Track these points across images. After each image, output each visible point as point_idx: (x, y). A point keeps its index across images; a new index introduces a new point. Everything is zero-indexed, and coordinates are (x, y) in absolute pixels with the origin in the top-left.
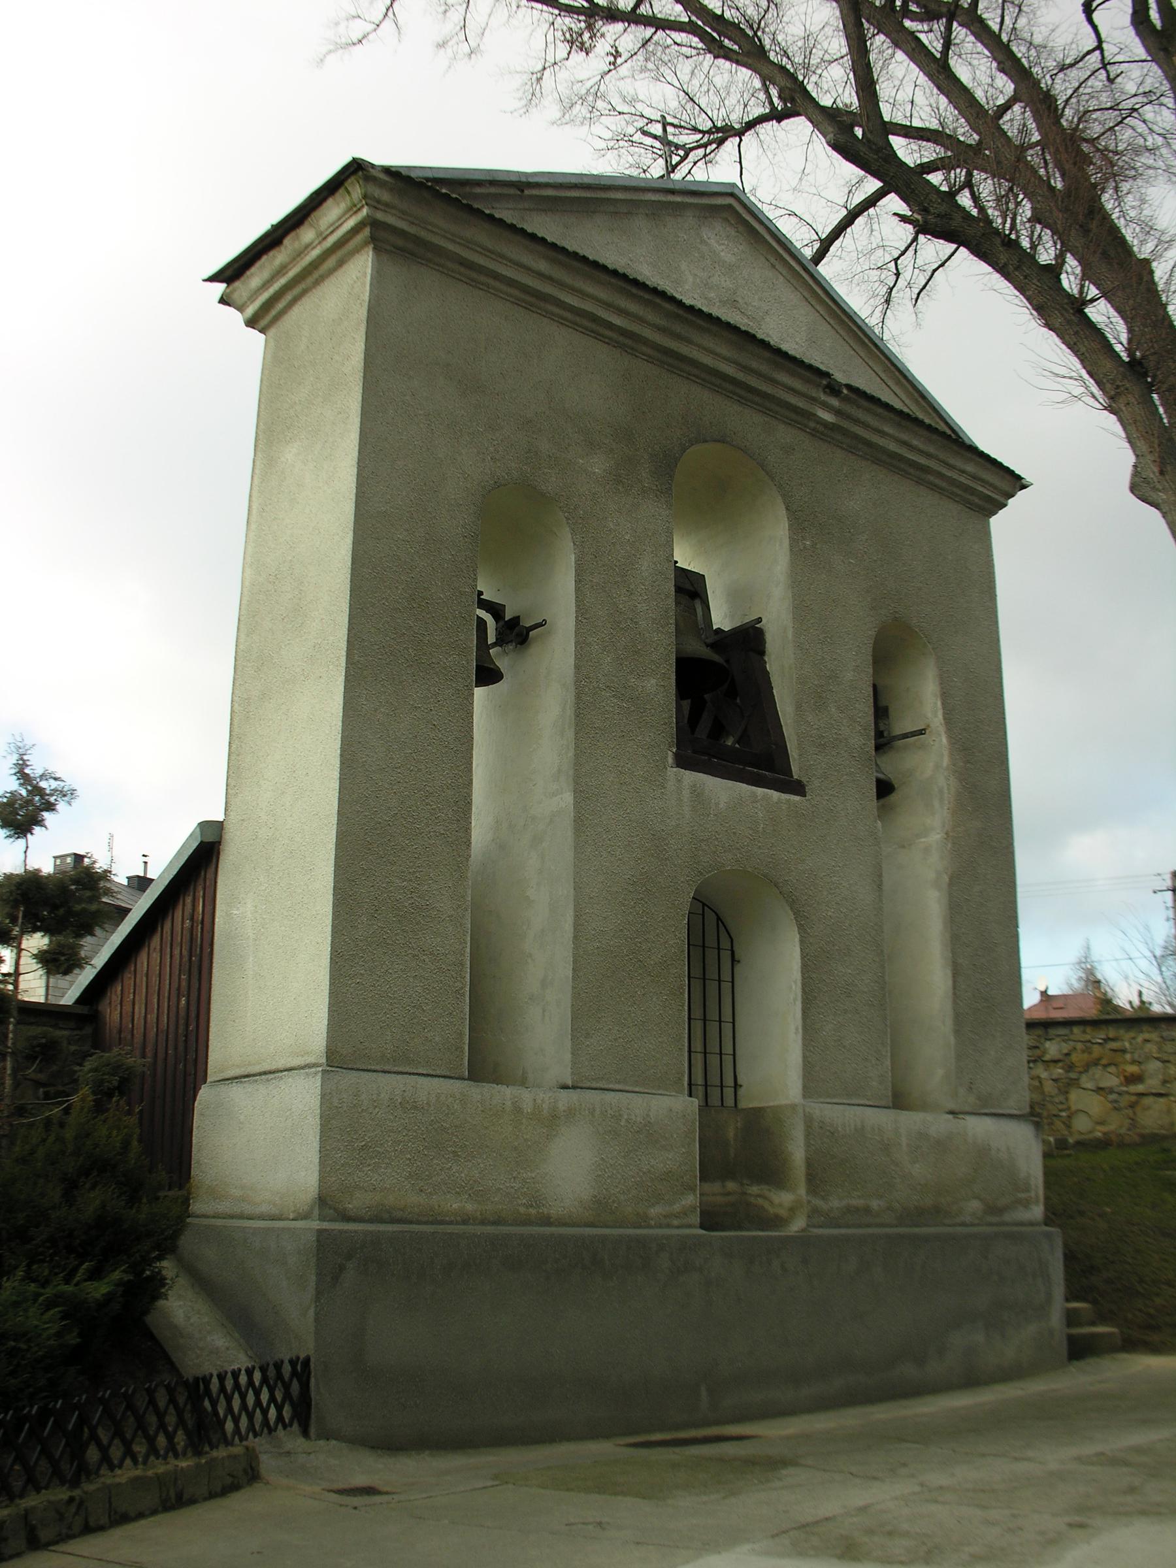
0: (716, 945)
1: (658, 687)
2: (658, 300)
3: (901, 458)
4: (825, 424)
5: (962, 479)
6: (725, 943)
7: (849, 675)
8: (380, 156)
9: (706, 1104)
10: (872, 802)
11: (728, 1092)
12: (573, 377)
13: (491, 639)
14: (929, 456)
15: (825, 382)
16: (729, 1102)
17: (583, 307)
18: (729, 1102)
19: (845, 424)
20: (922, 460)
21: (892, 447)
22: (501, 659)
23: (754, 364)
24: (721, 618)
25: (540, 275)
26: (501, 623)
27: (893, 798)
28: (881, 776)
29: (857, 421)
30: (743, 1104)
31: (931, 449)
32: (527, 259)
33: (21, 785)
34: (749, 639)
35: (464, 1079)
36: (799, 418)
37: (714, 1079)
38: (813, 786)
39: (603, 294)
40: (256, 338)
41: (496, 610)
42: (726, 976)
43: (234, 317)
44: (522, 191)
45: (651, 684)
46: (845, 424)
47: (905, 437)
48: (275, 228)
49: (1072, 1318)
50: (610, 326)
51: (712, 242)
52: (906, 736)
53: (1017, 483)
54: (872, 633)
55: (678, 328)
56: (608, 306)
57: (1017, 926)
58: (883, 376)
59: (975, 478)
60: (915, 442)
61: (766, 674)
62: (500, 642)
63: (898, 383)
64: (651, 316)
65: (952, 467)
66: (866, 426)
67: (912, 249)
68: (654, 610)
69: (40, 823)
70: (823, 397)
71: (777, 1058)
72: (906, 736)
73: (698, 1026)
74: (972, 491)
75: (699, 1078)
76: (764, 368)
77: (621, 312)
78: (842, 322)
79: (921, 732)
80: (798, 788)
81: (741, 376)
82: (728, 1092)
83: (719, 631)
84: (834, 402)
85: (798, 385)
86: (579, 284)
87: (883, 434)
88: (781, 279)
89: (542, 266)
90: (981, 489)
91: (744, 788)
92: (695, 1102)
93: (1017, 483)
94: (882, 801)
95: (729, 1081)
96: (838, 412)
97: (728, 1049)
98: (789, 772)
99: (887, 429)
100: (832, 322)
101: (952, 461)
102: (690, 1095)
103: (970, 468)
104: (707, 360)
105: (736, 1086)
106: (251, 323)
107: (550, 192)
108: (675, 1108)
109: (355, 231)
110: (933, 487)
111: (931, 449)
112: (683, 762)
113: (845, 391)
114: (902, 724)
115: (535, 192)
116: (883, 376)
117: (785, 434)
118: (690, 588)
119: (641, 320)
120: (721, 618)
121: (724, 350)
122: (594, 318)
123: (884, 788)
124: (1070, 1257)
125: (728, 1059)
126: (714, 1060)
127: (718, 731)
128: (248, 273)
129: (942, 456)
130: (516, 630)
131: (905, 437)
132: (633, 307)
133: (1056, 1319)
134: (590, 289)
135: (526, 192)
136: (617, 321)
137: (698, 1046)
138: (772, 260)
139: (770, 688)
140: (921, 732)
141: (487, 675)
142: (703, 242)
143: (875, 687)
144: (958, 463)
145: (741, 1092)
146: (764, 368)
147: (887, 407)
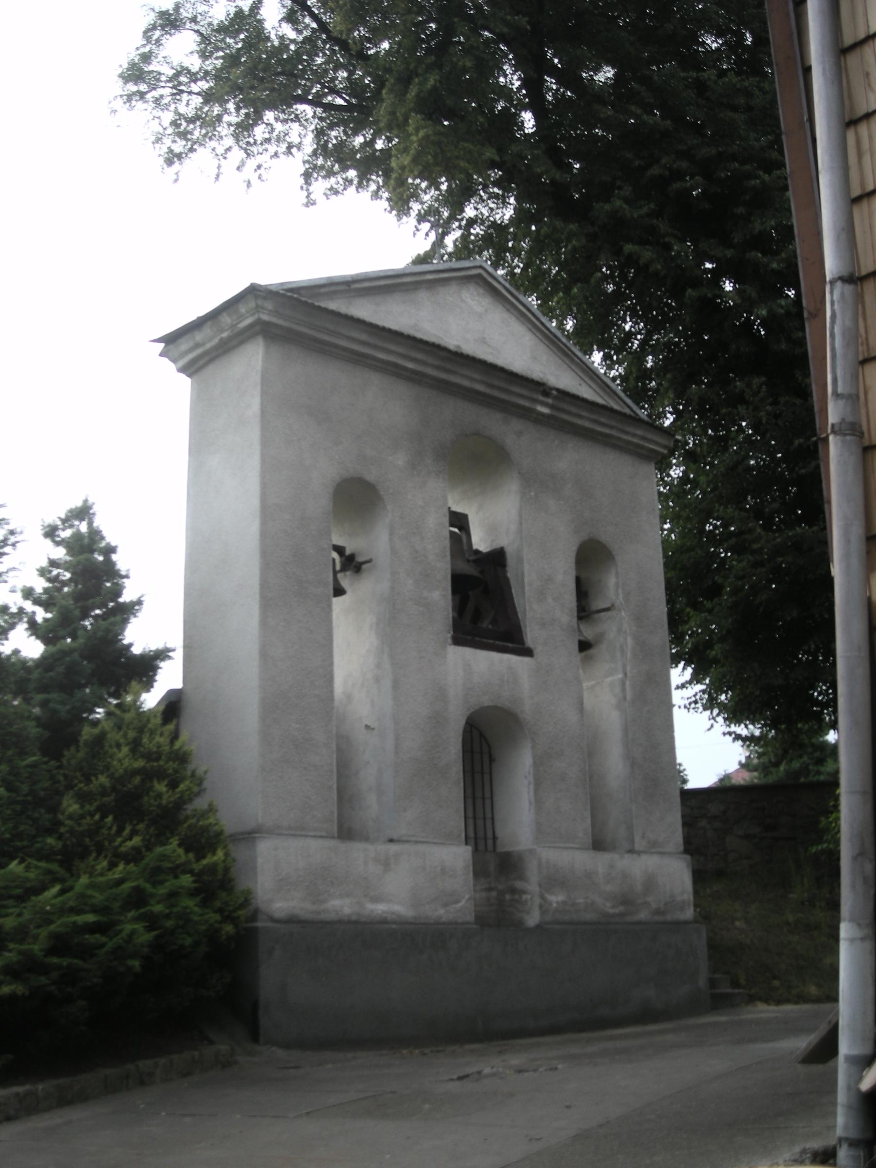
1: (441, 597)
3: (592, 431)
5: (635, 440)
8: (264, 280)
9: (476, 850)
10: (577, 657)
11: (490, 842)
13: (338, 568)
14: (611, 427)
16: (490, 848)
18: (490, 848)
19: (556, 414)
21: (587, 424)
22: (345, 581)
23: (496, 383)
24: (480, 541)
27: (591, 652)
28: (582, 638)
30: (500, 849)
31: (613, 423)
32: (355, 334)
35: (333, 838)
37: (481, 834)
38: (538, 650)
39: (400, 350)
41: (340, 550)
45: (436, 595)
46: (556, 414)
47: (595, 417)
49: (712, 983)
51: (469, 300)
52: (599, 611)
56: (404, 357)
59: (644, 438)
60: (603, 420)
61: (507, 580)
62: (344, 569)
64: (430, 360)
65: (627, 433)
66: (569, 413)
68: (437, 528)
70: (541, 398)
71: (520, 818)
72: (599, 611)
74: (643, 447)
75: (471, 834)
76: (502, 384)
78: (553, 343)
80: (528, 652)
81: (488, 391)
82: (490, 842)
83: (477, 552)
84: (550, 401)
85: (525, 392)
87: (580, 417)
89: (364, 337)
91: (495, 656)
92: (469, 848)
94: (585, 653)
95: (490, 834)
96: (552, 407)
97: (489, 815)
101: (627, 429)
104: (466, 383)
106: (182, 370)
107: (367, 284)
108: (457, 856)
111: (613, 423)
112: (458, 641)
117: (517, 424)
118: (459, 521)
120: (480, 541)
121: (476, 376)
122: (396, 365)
123: (584, 646)
126: (480, 823)
127: (477, 616)
130: (354, 564)
132: (420, 356)
133: (702, 983)
134: (393, 347)
136: (410, 365)
137: (470, 814)
139: (510, 588)
140: (607, 609)
141: (339, 591)
142: (463, 301)
144: (632, 430)
146: (502, 384)
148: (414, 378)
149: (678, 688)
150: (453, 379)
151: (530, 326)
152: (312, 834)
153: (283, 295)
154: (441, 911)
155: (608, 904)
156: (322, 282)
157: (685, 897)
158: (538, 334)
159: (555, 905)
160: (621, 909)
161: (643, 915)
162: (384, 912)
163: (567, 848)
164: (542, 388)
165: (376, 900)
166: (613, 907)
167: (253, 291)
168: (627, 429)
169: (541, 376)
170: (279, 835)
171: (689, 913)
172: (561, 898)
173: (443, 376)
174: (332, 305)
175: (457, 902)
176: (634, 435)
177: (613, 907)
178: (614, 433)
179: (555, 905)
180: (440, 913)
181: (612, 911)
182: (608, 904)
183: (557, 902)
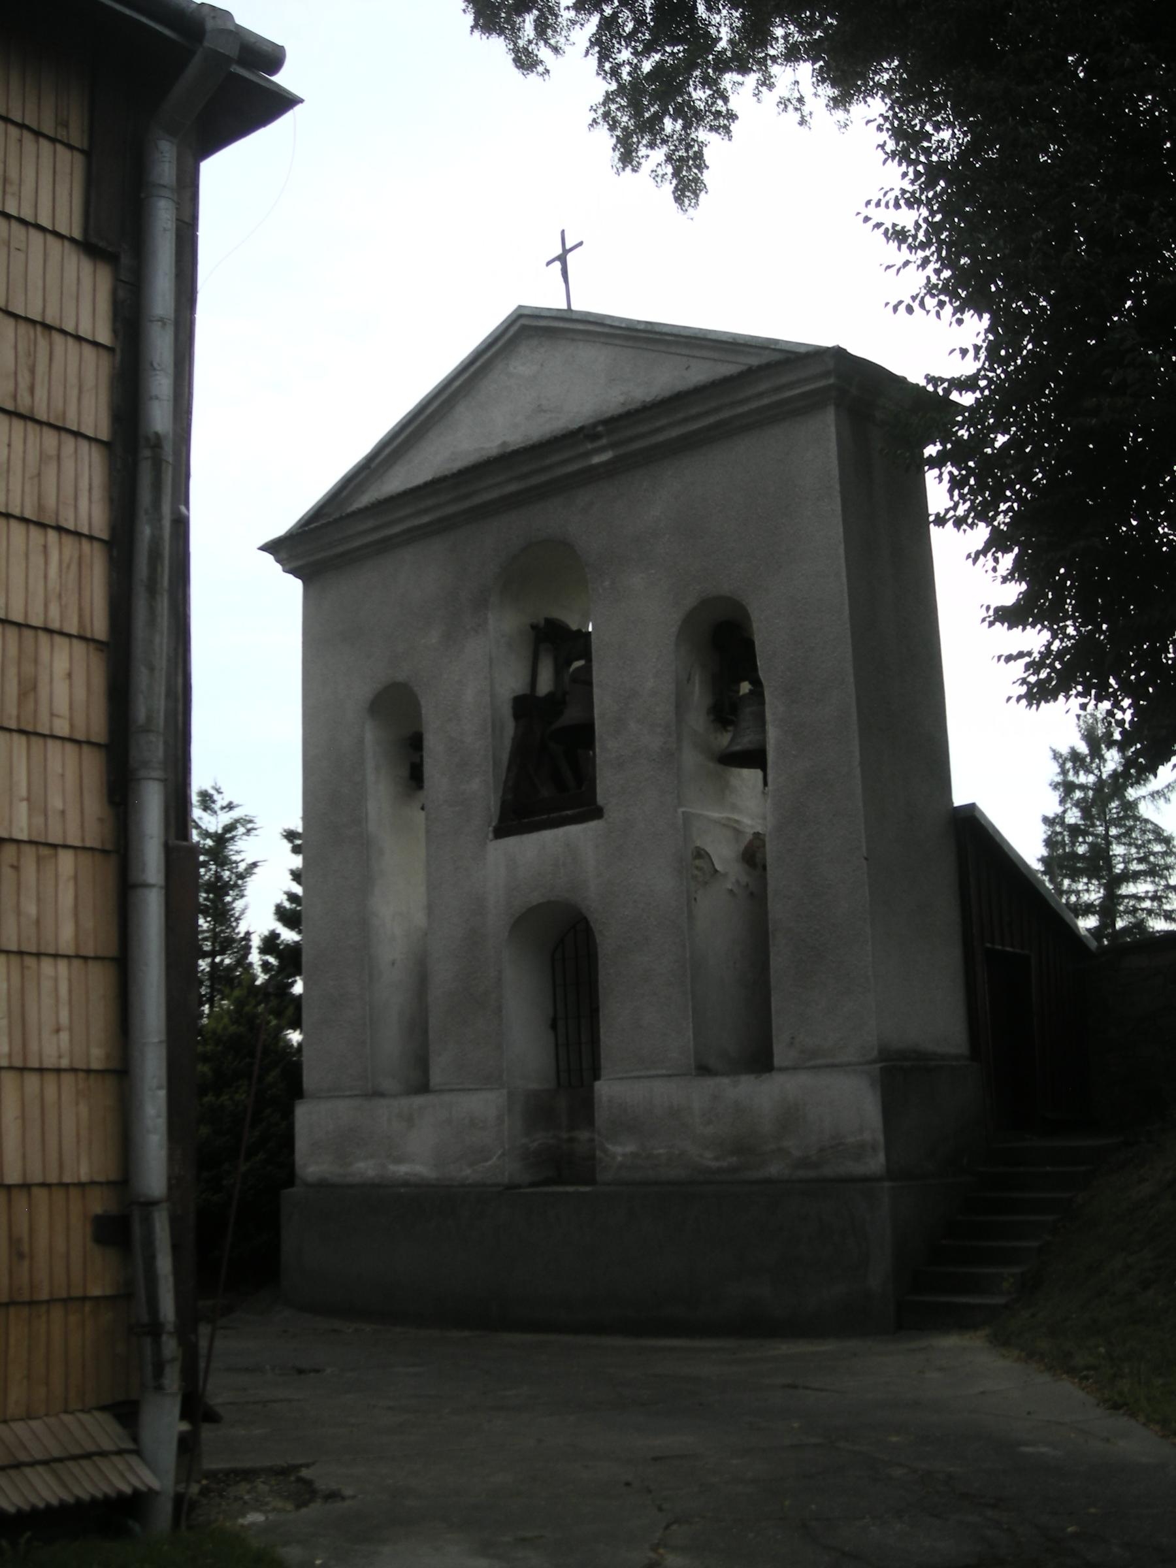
5: (766, 401)
14: (717, 410)
17: (166, 612)
20: (711, 420)
21: (674, 433)
29: (631, 440)
33: (1040, 653)
36: (591, 476)
46: (621, 451)
47: (680, 416)
53: (273, 548)
60: (693, 411)
66: (642, 436)
69: (252, 874)
70: (590, 446)
77: (426, 511)
78: (635, 339)
84: (604, 441)
89: (370, 523)
91: (547, 835)
93: (273, 548)
96: (612, 446)
99: (663, 422)
103: (764, 386)
104: (494, 494)
107: (387, 451)
115: (377, 461)
131: (680, 416)
132: (430, 502)
136: (425, 519)
148: (443, 526)
149: (223, 808)
150: (477, 500)
151: (602, 340)
152: (348, 1093)
153: (298, 534)
154: (468, 1171)
155: (708, 1155)
156: (724, 339)
157: (867, 1136)
158: (617, 342)
159: (619, 1158)
160: (733, 1160)
161: (774, 1169)
162: (406, 1174)
163: (639, 1077)
164: (581, 436)
165: (399, 1160)
166: (717, 1159)
167: (839, 354)
168: (548, 462)
169: (622, 399)
170: (319, 1098)
171: (876, 1163)
172: (630, 1148)
173: (467, 504)
174: (364, 500)
175: (487, 1160)
176: (760, 395)
177: (717, 1159)
178: (725, 414)
179: (619, 1158)
180: (467, 1173)
181: (714, 1164)
182: (708, 1155)
183: (624, 1155)
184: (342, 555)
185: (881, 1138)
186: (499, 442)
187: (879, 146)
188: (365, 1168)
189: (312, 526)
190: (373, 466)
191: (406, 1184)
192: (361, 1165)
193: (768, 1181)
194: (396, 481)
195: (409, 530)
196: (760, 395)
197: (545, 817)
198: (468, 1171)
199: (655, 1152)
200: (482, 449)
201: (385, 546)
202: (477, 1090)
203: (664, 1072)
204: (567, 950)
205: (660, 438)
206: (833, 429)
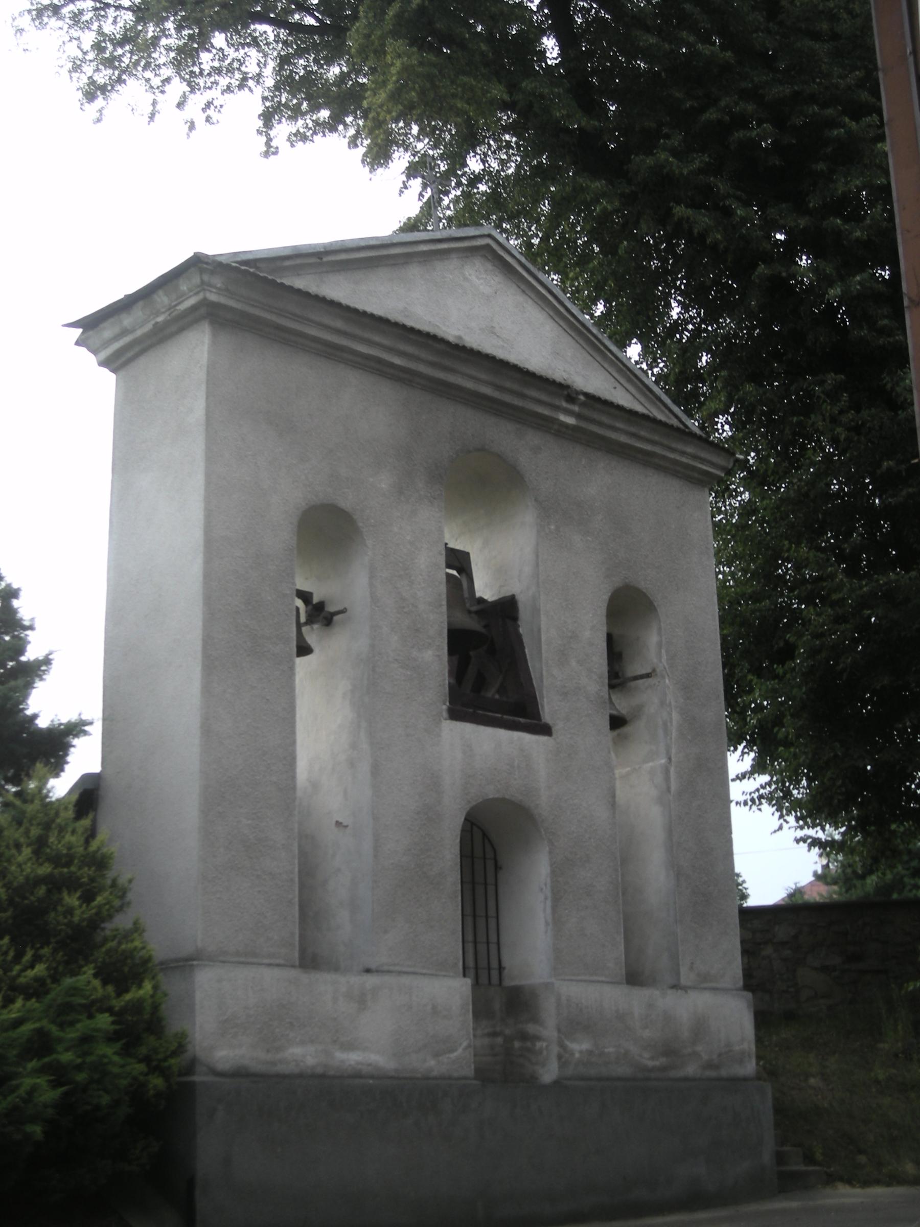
0: (485, 940)
1: (434, 658)
2: (430, 342)
4: (567, 426)
5: (684, 460)
6: (490, 855)
7: (587, 634)
9: (476, 984)
11: (495, 973)
12: (366, 412)
13: (303, 619)
15: (566, 393)
19: (583, 425)
20: (648, 447)
21: (623, 439)
22: (312, 636)
23: (508, 384)
25: (338, 332)
26: (310, 607)
27: (625, 730)
28: (614, 712)
30: (508, 983)
31: (656, 438)
34: (507, 608)
36: (546, 425)
37: (483, 963)
38: (558, 727)
40: (108, 379)
42: (490, 880)
43: (87, 358)
44: (321, 259)
45: (428, 655)
46: (583, 425)
47: (633, 429)
48: (127, 297)
49: (780, 1158)
50: (392, 365)
51: (473, 278)
52: (636, 678)
54: (606, 597)
55: (447, 362)
56: (390, 350)
57: (731, 833)
58: (616, 375)
59: (695, 457)
60: (643, 433)
61: (519, 637)
62: (310, 621)
63: (629, 380)
64: (423, 354)
66: (600, 424)
67: (486, 841)
70: (564, 404)
71: (533, 943)
72: (636, 678)
73: (469, 921)
74: (694, 468)
75: (471, 963)
76: (516, 387)
78: (580, 333)
79: (648, 676)
80: (545, 730)
81: (496, 394)
82: (495, 973)
83: (481, 601)
84: (576, 408)
85: (543, 397)
86: (367, 335)
87: (616, 429)
88: (530, 302)
89: (339, 324)
90: (700, 466)
91: (503, 734)
92: (468, 981)
95: (494, 964)
96: (578, 416)
97: (493, 938)
98: (539, 719)
99: (619, 425)
100: (573, 334)
101: (674, 445)
102: (464, 976)
103: (690, 449)
104: (469, 385)
105: (501, 968)
106: (104, 363)
108: (453, 991)
109: (194, 308)
110: (658, 468)
112: (455, 714)
113: (582, 397)
114: (635, 668)
116: (616, 375)
117: (533, 438)
118: (458, 561)
119: (417, 359)
123: (617, 722)
124: (779, 1110)
125: (493, 947)
126: (482, 948)
127: (480, 683)
128: (102, 326)
129: (666, 442)
130: (323, 614)
131: (633, 429)
132: (410, 349)
133: (767, 1157)
134: (377, 338)
135: (325, 259)
136: (397, 361)
138: (523, 287)
140: (648, 676)
141: (304, 650)
142: (466, 279)
143: (610, 638)
145: (506, 972)
146: (516, 387)
147: (620, 408)
152: (266, 961)
154: (432, 1063)
155: (646, 1055)
157: (745, 1046)
159: (577, 1055)
160: (662, 1061)
161: (691, 1070)
165: (349, 1047)
166: (652, 1058)
171: (750, 1067)
172: (586, 1046)
174: (299, 283)
175: (452, 1051)
176: (683, 453)
177: (652, 1058)
178: (658, 450)
181: (650, 1064)
182: (646, 1055)
183: (581, 1052)
184: (279, 328)
185: (753, 1047)
186: (457, 333)
187: (275, 153)
188: (302, 1055)
189: (243, 268)
190: (325, 259)
191: (358, 1075)
192: (296, 1051)
193: (686, 1079)
194: (339, 289)
195: (379, 361)
196: (683, 453)
197: (499, 715)
198: (432, 1063)
199: (606, 1050)
200: (438, 327)
201: (331, 353)
202: (432, 975)
203: (603, 979)
204: (488, 844)
205: (614, 435)
206: (206, 355)
